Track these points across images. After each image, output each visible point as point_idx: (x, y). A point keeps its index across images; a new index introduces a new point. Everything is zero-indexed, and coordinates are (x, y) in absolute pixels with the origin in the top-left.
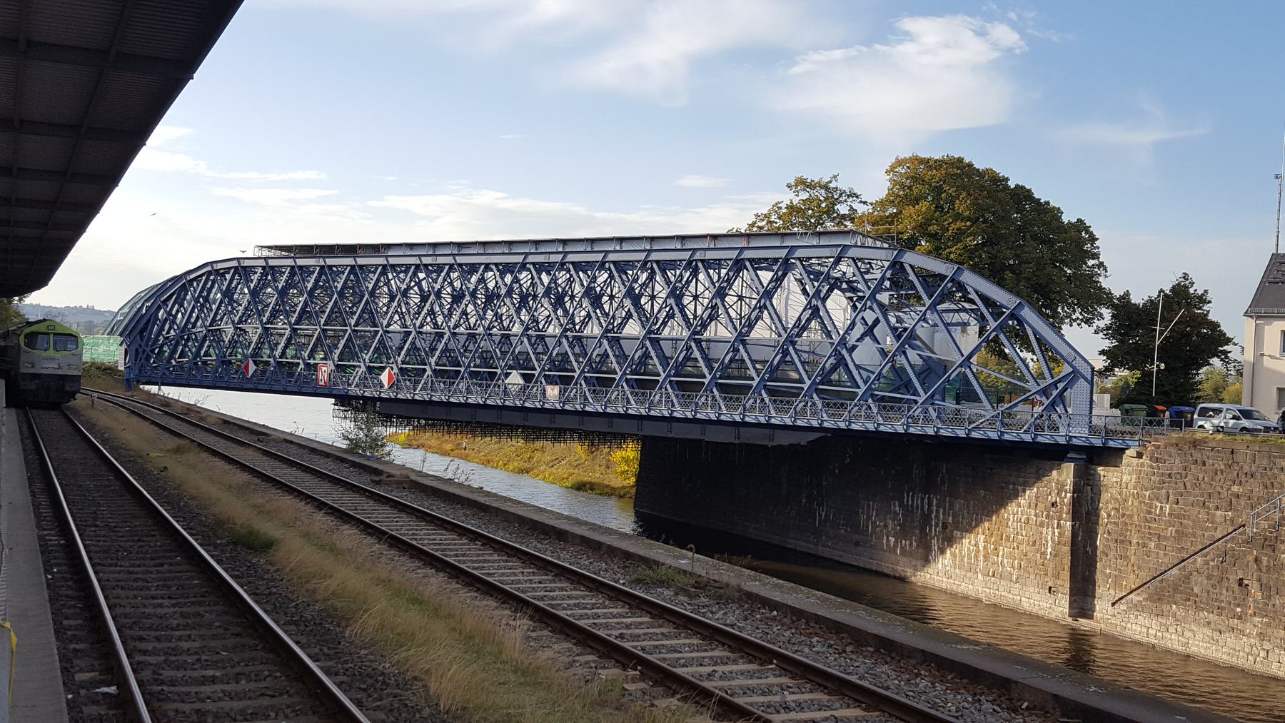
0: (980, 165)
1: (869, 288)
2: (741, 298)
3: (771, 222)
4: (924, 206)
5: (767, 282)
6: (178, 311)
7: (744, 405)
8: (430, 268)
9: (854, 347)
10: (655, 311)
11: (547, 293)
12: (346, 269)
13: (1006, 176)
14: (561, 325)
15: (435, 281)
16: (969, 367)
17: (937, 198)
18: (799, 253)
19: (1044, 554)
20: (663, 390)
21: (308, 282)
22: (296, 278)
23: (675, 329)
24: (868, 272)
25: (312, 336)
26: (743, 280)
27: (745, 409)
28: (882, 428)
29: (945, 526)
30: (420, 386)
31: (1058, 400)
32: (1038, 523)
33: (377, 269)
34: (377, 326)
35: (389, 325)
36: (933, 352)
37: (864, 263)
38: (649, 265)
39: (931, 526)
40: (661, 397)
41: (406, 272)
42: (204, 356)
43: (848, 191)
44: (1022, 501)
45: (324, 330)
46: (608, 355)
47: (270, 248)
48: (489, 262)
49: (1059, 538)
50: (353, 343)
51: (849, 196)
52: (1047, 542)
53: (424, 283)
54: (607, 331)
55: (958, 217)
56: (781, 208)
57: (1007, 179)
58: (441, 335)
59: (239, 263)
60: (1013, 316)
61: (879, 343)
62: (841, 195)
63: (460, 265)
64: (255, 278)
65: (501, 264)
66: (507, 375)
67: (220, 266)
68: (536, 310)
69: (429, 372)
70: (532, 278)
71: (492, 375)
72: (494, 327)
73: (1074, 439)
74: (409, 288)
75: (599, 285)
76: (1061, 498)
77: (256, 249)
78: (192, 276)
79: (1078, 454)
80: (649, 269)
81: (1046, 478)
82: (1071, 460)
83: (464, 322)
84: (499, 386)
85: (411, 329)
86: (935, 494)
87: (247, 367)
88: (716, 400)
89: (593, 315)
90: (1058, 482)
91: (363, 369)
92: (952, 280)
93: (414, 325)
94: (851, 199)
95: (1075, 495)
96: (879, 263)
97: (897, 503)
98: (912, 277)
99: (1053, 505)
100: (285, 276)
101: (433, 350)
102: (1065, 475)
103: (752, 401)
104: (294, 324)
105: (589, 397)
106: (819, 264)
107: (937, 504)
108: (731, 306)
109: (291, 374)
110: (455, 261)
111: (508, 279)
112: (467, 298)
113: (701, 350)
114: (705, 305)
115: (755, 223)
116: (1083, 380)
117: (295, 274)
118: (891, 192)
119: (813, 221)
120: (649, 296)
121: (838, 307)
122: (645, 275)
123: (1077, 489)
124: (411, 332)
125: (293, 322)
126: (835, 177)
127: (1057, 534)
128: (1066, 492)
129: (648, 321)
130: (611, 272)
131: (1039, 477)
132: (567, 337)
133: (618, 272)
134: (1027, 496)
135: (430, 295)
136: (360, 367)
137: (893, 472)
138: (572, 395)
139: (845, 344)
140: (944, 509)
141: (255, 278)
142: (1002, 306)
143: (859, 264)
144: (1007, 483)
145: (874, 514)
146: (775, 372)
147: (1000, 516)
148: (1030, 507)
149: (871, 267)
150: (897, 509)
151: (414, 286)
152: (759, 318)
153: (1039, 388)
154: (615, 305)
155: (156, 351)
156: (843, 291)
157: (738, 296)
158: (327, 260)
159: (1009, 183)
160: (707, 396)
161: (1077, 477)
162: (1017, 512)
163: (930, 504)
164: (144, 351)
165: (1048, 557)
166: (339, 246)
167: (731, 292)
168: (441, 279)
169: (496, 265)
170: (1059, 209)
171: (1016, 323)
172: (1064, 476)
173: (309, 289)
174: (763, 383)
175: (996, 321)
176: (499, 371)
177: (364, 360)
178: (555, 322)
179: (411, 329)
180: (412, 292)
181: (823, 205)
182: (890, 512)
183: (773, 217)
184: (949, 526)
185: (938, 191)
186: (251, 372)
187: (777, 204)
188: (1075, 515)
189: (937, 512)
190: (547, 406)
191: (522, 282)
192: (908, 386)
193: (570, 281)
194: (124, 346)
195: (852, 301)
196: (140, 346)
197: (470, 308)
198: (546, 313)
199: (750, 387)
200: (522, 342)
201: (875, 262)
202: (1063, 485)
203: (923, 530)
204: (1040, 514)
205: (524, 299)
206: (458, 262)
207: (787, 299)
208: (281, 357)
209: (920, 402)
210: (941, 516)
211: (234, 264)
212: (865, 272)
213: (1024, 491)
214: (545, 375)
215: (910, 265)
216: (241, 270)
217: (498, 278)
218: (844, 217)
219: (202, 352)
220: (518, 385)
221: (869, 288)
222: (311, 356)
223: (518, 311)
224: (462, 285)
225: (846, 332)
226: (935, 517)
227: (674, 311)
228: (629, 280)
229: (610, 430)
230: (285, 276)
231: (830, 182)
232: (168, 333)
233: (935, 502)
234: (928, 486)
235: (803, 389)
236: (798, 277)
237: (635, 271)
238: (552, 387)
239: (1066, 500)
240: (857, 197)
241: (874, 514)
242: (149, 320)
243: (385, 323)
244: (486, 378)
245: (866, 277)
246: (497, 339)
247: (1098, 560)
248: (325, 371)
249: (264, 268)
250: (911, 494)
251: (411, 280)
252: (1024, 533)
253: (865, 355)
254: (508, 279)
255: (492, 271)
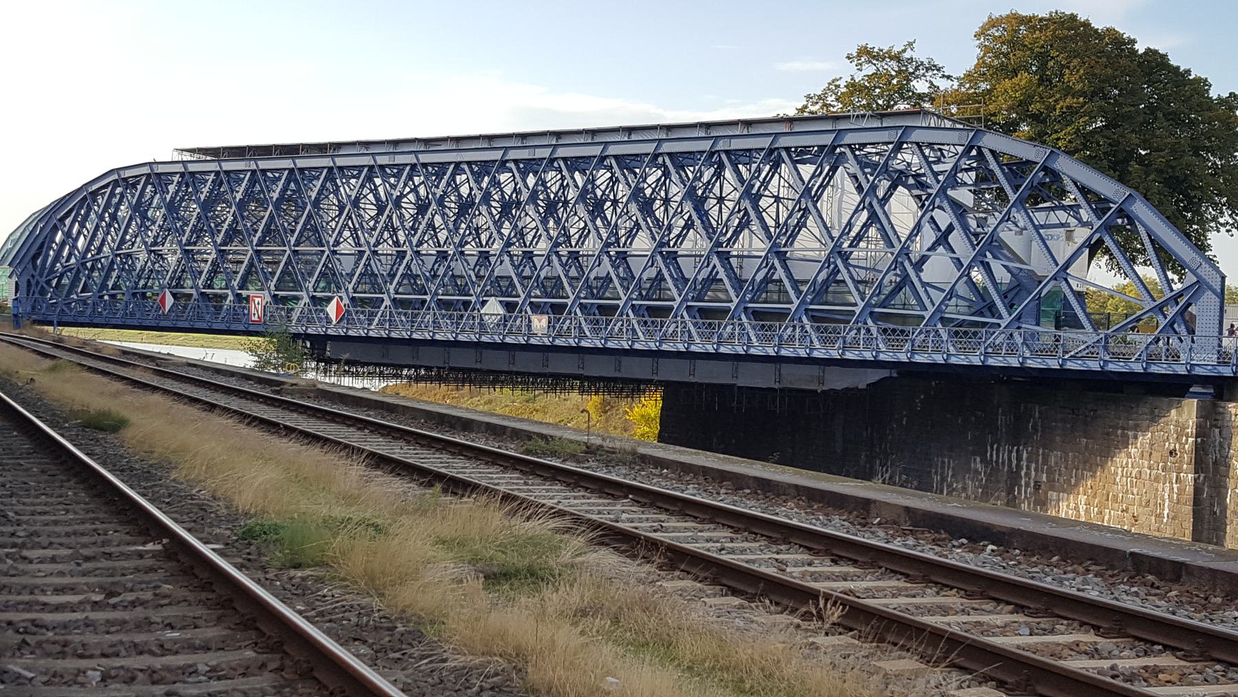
0: (1098, 24)
1: (938, 182)
2: (777, 199)
3: (825, 105)
4: (1023, 78)
5: (809, 176)
6: (79, 233)
7: (844, 338)
8: (388, 171)
9: (924, 259)
10: (725, 218)
11: (582, 197)
12: (321, 173)
13: (1132, 37)
14: (551, 238)
15: (393, 187)
16: (1066, 280)
17: (1043, 66)
18: (849, 139)
19: (1160, 516)
20: (679, 318)
21: (202, 193)
22: (258, 188)
23: (695, 242)
24: (938, 161)
25: (278, 263)
26: (780, 176)
27: (844, 342)
28: (953, 360)
29: (1037, 486)
30: (377, 319)
31: (1179, 319)
32: (1153, 478)
33: (360, 172)
34: (323, 246)
35: (337, 243)
36: (1022, 262)
37: (933, 149)
38: (660, 160)
39: (1020, 486)
40: (734, 329)
41: (398, 176)
42: (112, 289)
43: (926, 63)
44: (1133, 451)
45: (258, 252)
46: (611, 280)
47: (192, 151)
48: (459, 159)
49: (1178, 495)
50: (293, 267)
51: (927, 69)
52: (1164, 500)
53: (381, 189)
54: (661, 244)
55: (1068, 91)
56: (838, 86)
57: (1133, 42)
58: (401, 255)
59: (152, 169)
60: (1121, 212)
61: (954, 252)
62: (917, 68)
63: (425, 165)
64: (172, 188)
65: (475, 162)
66: (484, 303)
67: (128, 174)
68: (567, 220)
69: (387, 302)
70: (563, 178)
71: (466, 304)
72: (467, 243)
73: (1197, 368)
74: (402, 196)
75: (650, 186)
76: (1180, 444)
77: (176, 153)
78: (94, 187)
79: (1204, 388)
80: (715, 163)
81: (1163, 420)
82: (1195, 395)
83: (474, 239)
84: (474, 317)
85: (365, 248)
86: (1025, 445)
87: (163, 300)
88: (806, 332)
89: (642, 223)
90: (1177, 424)
91: (306, 300)
92: (1045, 168)
93: (411, 242)
94: (930, 73)
95: (1199, 440)
96: (952, 149)
97: (978, 459)
98: (993, 165)
99: (1171, 453)
100: (244, 185)
101: (392, 276)
102: (1186, 414)
103: (790, 329)
104: (220, 245)
105: (638, 330)
106: (877, 154)
107: (1027, 459)
108: (764, 210)
109: (219, 309)
110: (418, 160)
111: (531, 180)
112: (434, 206)
113: (729, 269)
114: (731, 208)
115: (806, 107)
116: (1210, 293)
117: (221, 183)
118: (981, 62)
119: (880, 102)
120: (717, 198)
121: (906, 211)
122: (712, 170)
123: (1201, 432)
124: (405, 252)
125: (219, 241)
126: (910, 44)
127: (1176, 490)
128: (1187, 437)
129: (714, 233)
130: (666, 167)
131: (1154, 418)
132: (661, 253)
133: (621, 169)
134: (1139, 445)
135: (430, 204)
136: (297, 299)
137: (973, 419)
138: (616, 329)
139: (907, 254)
140: (1037, 463)
141: (172, 188)
142: (1107, 200)
143: (927, 152)
144: (1116, 427)
145: (950, 474)
146: (821, 291)
147: (1106, 471)
148: (1142, 456)
149: (942, 154)
150: (979, 465)
151: (408, 193)
152: (801, 225)
153: (1154, 304)
154: (671, 212)
155: (54, 282)
156: (909, 188)
157: (774, 196)
158: (259, 162)
159: (1136, 47)
160: (794, 327)
161: (1201, 417)
162: (1127, 464)
163: (1019, 459)
164: (38, 283)
165: (1165, 521)
166: (277, 146)
167: (767, 193)
168: (444, 182)
169: (469, 163)
170: (1206, 80)
171: (1126, 221)
172: (1185, 416)
173: (274, 199)
174: (869, 310)
175: (1100, 219)
176: (473, 299)
177: (347, 290)
178: (593, 233)
179: (365, 248)
180: (405, 200)
181: (895, 82)
182: (969, 471)
183: (830, 99)
184: (1043, 487)
185: (1043, 58)
186: (168, 306)
187: (833, 81)
188: (1199, 465)
189: (1028, 468)
190: (533, 341)
191: (549, 185)
192: (991, 309)
193: (614, 181)
194: (15, 279)
195: (921, 200)
196: (33, 276)
197: (438, 221)
198: (533, 225)
199: (671, 308)
200: (502, 262)
201: (946, 148)
202: (1184, 428)
203: (1010, 491)
204: (1155, 465)
205: (551, 208)
206: (338, 164)
207: (840, 200)
208: (240, 288)
209: (1003, 325)
210: (1033, 473)
211: (146, 170)
212: (934, 162)
213: (1136, 437)
214: (531, 303)
215: (992, 152)
216: (155, 176)
217: (518, 179)
218: (921, 97)
219: (110, 284)
220: (497, 315)
221: (938, 182)
222: (243, 286)
223: (544, 221)
224: (428, 193)
225: (909, 237)
226: (1026, 474)
227: (749, 217)
228: (689, 179)
229: (617, 375)
230: (244, 185)
231: (904, 51)
232: (67, 261)
233: (1025, 455)
234: (1017, 436)
235: (923, 318)
236: (852, 171)
237: (697, 167)
238: (539, 317)
239: (1187, 446)
240: (939, 70)
241: (950, 474)
242: (43, 244)
243: (332, 241)
244: (456, 308)
245: (936, 168)
246: (473, 260)
247: (1228, 522)
248: (259, 301)
249: (182, 175)
250: (995, 446)
251: (405, 185)
252: (1135, 491)
253: (939, 270)
254: (531, 180)
255: (511, 171)
